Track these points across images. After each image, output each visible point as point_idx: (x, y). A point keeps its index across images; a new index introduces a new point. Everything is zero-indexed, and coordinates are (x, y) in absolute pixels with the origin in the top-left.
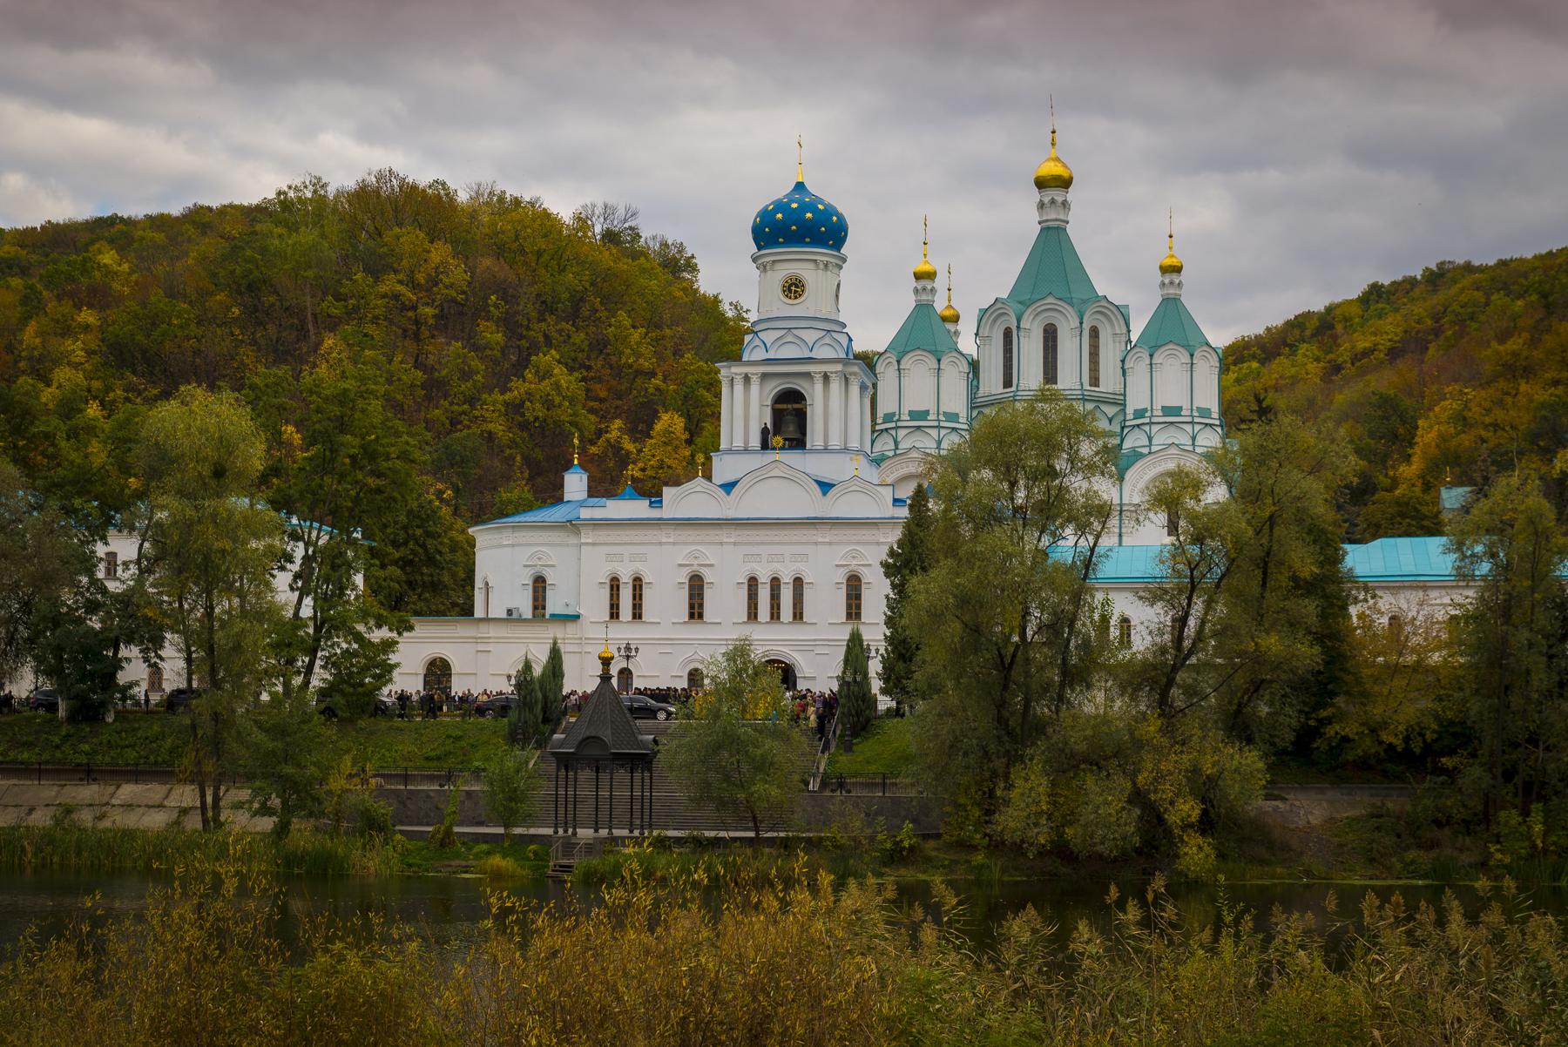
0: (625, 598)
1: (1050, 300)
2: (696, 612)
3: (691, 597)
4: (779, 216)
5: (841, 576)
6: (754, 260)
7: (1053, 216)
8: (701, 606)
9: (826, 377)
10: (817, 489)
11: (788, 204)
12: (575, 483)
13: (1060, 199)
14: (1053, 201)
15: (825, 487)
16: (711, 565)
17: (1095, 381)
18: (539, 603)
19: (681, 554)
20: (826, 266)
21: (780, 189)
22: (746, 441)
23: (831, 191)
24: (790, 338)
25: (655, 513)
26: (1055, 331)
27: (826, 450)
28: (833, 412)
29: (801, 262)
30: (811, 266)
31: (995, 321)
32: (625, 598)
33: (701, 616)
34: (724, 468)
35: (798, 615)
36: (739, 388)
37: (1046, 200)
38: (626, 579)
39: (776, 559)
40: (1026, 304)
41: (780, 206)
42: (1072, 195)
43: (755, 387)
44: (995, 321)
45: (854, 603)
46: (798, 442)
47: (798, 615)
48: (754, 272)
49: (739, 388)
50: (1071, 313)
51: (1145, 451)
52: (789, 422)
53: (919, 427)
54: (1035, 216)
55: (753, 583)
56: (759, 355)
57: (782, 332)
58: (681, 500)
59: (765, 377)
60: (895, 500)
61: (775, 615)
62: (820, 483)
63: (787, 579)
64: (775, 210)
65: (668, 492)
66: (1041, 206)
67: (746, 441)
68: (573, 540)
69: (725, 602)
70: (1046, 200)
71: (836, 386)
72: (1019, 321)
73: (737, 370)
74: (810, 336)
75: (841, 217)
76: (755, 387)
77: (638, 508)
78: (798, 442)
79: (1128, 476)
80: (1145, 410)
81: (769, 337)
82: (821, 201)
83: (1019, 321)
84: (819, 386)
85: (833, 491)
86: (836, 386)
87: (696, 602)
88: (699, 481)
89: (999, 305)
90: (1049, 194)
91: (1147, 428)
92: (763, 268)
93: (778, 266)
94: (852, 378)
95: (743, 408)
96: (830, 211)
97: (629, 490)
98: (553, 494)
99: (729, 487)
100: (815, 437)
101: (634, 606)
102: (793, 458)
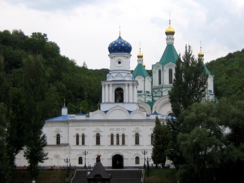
0: (80, 139)
1: (171, 63)
2: (98, 143)
3: (136, 139)
4: (116, 45)
5: (134, 134)
6: (109, 55)
8: (138, 141)
9: (128, 85)
10: (128, 113)
11: (118, 42)
12: (64, 111)
13: (172, 38)
14: (170, 38)
15: (130, 112)
16: (102, 131)
18: (58, 142)
21: (114, 38)
22: (109, 100)
23: (127, 39)
24: (119, 75)
25: (88, 119)
27: (129, 103)
28: (129, 94)
29: (120, 57)
30: (124, 57)
31: (168, 66)
32: (80, 139)
34: (103, 107)
35: (83, 143)
36: (107, 88)
37: (169, 38)
38: (80, 134)
41: (115, 42)
42: (175, 36)
43: (111, 88)
45: (83, 140)
46: (121, 101)
48: (109, 59)
49: (107, 88)
52: (119, 96)
53: (140, 95)
54: (166, 42)
55: (112, 136)
56: (111, 79)
57: (117, 74)
58: (94, 115)
59: (113, 85)
60: (147, 115)
61: (118, 143)
63: (121, 134)
64: (115, 44)
65: (91, 113)
66: (167, 39)
67: (109, 100)
68: (67, 125)
69: (105, 140)
72: (163, 68)
73: (106, 83)
74: (124, 75)
76: (111, 88)
77: (83, 117)
78: (121, 101)
81: (114, 75)
82: (126, 41)
83: (163, 68)
84: (127, 87)
86: (131, 87)
87: (112, 140)
88: (98, 110)
89: (157, 64)
92: (112, 58)
93: (115, 57)
94: (135, 85)
95: (108, 94)
96: (128, 44)
97: (81, 113)
98: (59, 114)
99: (106, 112)
100: (126, 99)
101: (82, 141)
102: (121, 105)
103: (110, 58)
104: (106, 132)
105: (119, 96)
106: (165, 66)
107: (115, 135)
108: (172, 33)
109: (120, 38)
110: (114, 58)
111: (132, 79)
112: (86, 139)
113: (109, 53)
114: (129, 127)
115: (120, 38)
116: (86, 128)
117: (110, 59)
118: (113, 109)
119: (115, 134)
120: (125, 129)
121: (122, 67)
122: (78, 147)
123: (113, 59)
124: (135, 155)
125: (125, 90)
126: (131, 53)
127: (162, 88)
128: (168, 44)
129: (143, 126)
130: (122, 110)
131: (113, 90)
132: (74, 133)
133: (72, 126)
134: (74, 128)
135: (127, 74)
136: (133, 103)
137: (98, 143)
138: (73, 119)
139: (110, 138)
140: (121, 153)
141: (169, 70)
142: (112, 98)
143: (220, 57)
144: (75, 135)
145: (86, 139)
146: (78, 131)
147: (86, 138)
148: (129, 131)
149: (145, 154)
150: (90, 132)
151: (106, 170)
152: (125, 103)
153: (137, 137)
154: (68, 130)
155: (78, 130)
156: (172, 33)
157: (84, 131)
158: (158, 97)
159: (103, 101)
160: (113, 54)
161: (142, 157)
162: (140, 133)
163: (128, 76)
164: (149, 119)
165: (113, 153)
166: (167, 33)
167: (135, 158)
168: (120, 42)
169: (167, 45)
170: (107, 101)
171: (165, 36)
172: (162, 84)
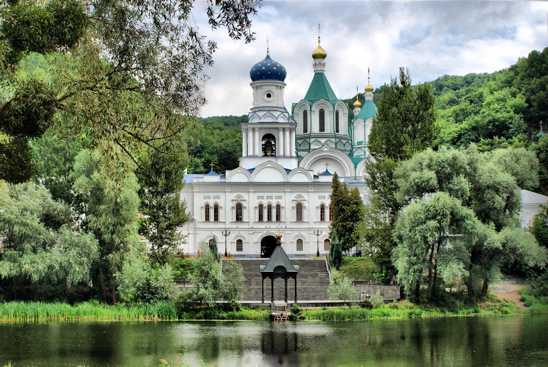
1: (322, 100)
2: (239, 218)
4: (264, 68)
5: (234, 204)
6: (251, 85)
7: (319, 69)
9: (254, 129)
13: (322, 63)
14: (320, 63)
15: (288, 171)
16: (245, 200)
17: (337, 131)
19: (233, 196)
20: (280, 87)
22: (284, 153)
25: (223, 180)
26: (324, 111)
27: (284, 157)
29: (269, 86)
30: (275, 87)
31: (300, 107)
33: (241, 219)
34: (245, 164)
35: (216, 218)
36: (250, 134)
37: (317, 63)
38: (212, 205)
39: (270, 198)
40: (313, 102)
42: (326, 60)
44: (300, 107)
47: (216, 218)
49: (250, 134)
50: (330, 105)
51: (363, 157)
52: (269, 146)
59: (260, 129)
60: (314, 176)
62: (286, 170)
65: (227, 172)
66: (315, 65)
69: (250, 214)
70: (317, 63)
71: (287, 133)
72: (311, 108)
73: (249, 126)
75: (285, 70)
76: (257, 134)
77: (213, 178)
79: (358, 166)
80: (362, 142)
83: (311, 108)
85: (291, 173)
86: (287, 133)
90: (318, 61)
91: (363, 149)
92: (256, 88)
93: (262, 87)
95: (252, 143)
99: (251, 170)
103: (253, 88)
104: (251, 201)
105: (269, 146)
106: (315, 104)
107: (211, 206)
108: (324, 56)
109: (268, 57)
110: (260, 88)
111: (287, 121)
112: (282, 212)
113: (251, 81)
114: (310, 194)
115: (268, 57)
116: (222, 195)
117: (252, 90)
118: (263, 167)
119: (265, 205)
120: (280, 197)
121: (273, 102)
122: (261, 226)
123: (259, 90)
124: (297, 236)
125: (279, 137)
126: (286, 81)
127: (310, 137)
128: (317, 72)
129: (308, 192)
130: (277, 168)
131: (259, 138)
132: (203, 203)
133: (199, 192)
134: (202, 195)
135: (280, 113)
136: (291, 157)
137: (239, 218)
138: (201, 180)
139: (204, 211)
140: (275, 234)
141: (320, 112)
142: (259, 151)
143: (216, 116)
144: (257, 206)
145: (221, 212)
146: (262, 200)
147: (305, 210)
148: (287, 201)
149: (226, 235)
150: (226, 201)
151: (290, 259)
152: (280, 157)
153: (299, 208)
154: (193, 198)
155: (209, 197)
156: (324, 56)
157: (217, 200)
158: (304, 150)
159: (244, 154)
160: (259, 83)
161: (220, 238)
162: (305, 204)
163: (282, 115)
164: (318, 182)
165: (262, 234)
166: (315, 57)
167: (235, 242)
168: (269, 64)
169: (313, 74)
170: (251, 153)
171: (312, 61)
172: (309, 132)
